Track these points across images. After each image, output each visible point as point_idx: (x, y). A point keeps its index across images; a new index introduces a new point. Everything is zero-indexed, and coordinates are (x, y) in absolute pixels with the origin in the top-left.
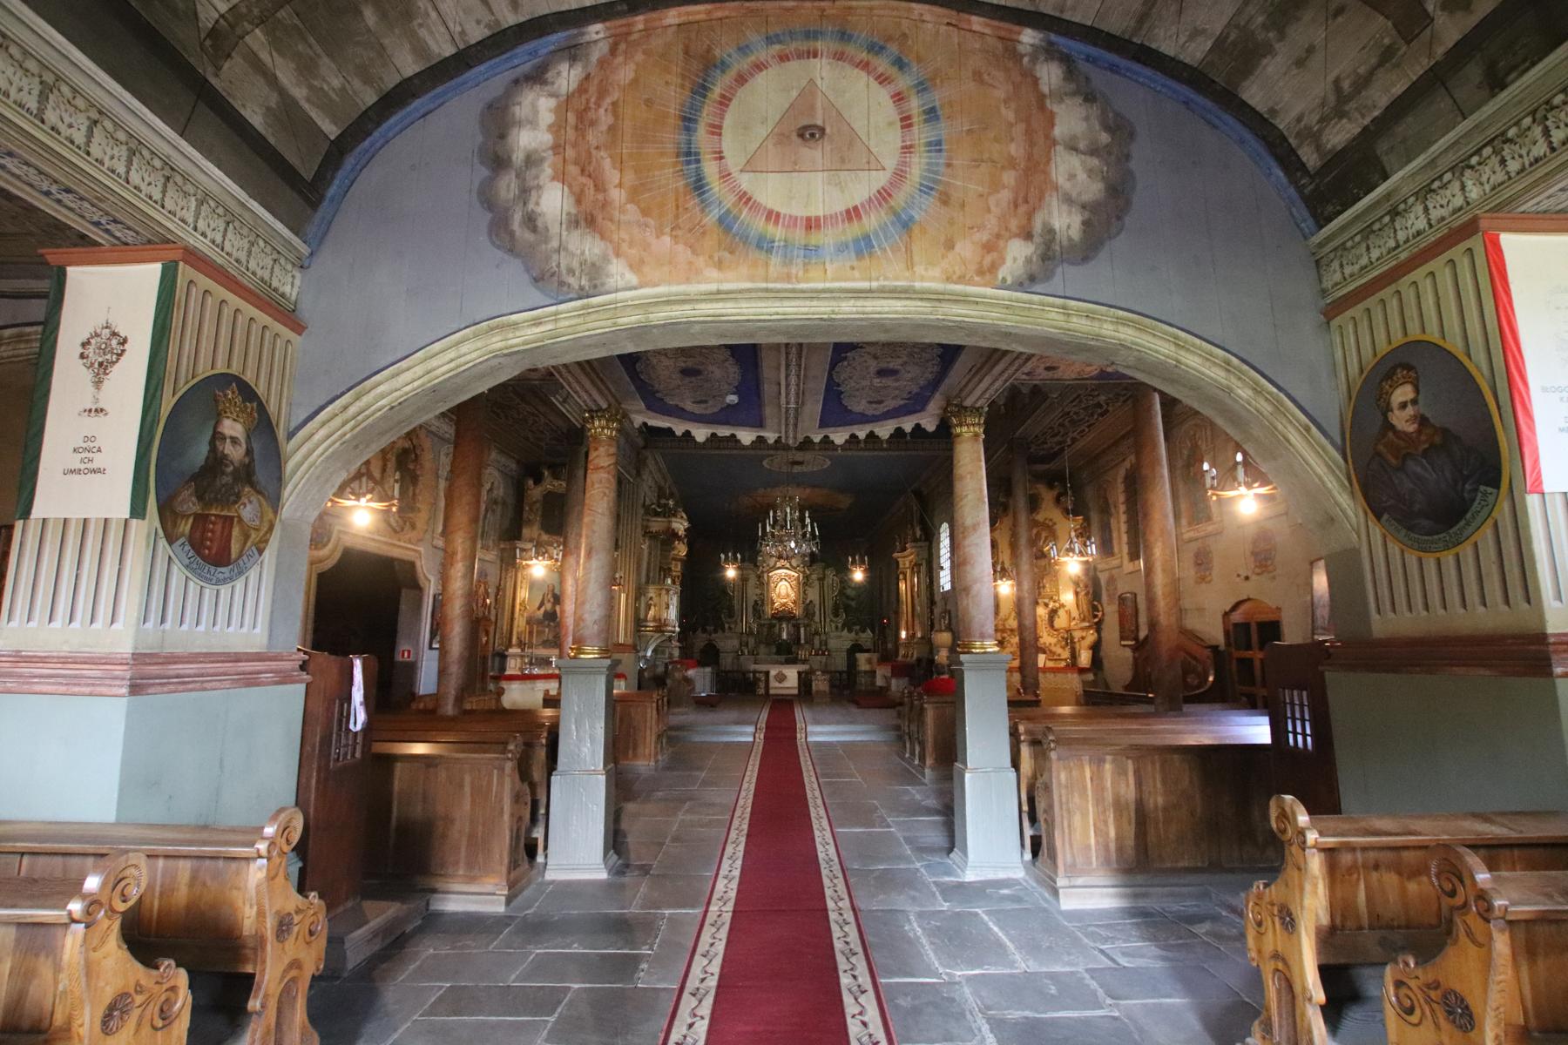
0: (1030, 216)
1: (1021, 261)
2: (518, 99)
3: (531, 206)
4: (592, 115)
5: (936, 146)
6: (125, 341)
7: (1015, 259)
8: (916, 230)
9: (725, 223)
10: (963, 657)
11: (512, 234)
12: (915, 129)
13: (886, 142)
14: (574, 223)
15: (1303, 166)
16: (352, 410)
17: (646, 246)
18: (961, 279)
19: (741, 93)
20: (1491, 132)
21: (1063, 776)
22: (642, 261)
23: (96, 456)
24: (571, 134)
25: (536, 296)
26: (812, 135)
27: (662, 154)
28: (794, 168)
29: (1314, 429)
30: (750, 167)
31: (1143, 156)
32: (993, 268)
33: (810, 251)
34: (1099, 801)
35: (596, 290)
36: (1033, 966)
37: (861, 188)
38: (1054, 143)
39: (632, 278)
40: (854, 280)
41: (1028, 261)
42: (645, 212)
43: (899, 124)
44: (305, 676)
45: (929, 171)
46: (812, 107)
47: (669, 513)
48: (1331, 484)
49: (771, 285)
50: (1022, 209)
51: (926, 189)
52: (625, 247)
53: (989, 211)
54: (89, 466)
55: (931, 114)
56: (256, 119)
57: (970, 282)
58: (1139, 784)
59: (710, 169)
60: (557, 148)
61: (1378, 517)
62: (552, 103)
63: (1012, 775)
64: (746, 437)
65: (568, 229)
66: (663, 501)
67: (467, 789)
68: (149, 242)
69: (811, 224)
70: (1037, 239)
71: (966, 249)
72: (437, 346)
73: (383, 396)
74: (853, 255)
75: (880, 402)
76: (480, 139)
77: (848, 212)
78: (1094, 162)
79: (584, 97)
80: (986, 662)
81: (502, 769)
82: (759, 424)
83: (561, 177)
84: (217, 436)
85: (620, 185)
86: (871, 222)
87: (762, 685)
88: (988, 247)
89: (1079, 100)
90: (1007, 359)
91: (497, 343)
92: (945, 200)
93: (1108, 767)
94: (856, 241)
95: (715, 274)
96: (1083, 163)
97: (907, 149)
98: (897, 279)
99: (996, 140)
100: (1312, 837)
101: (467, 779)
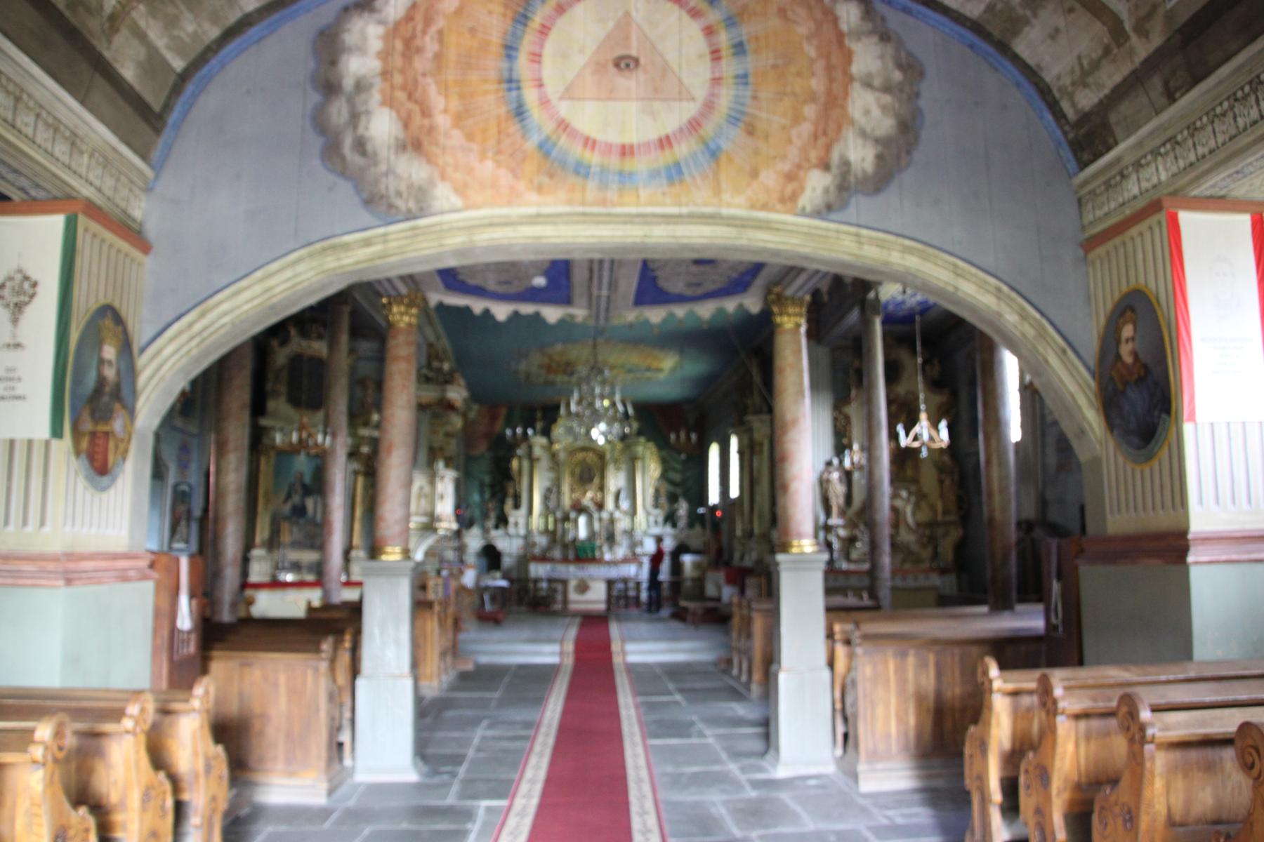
0: (828, 148)
1: (819, 191)
2: (348, 26)
3: (361, 131)
4: (418, 42)
5: (743, 79)
6: (35, 285)
7: (814, 189)
8: (723, 159)
9: (545, 148)
10: (780, 557)
11: (343, 158)
12: (724, 62)
13: (697, 75)
14: (402, 147)
15: (1064, 116)
16: (198, 327)
17: (470, 171)
18: (765, 207)
19: (561, 22)
20: (1169, 133)
21: (868, 670)
22: (466, 185)
23: (18, 385)
24: (398, 61)
25: (365, 217)
26: (628, 66)
27: (486, 81)
28: (611, 95)
29: (1070, 353)
30: (569, 94)
31: (931, 94)
32: (794, 197)
33: (625, 177)
34: (902, 691)
35: (422, 212)
36: (822, 826)
37: (673, 118)
38: (851, 79)
39: (457, 201)
40: (664, 204)
41: (826, 191)
42: (470, 137)
43: (708, 57)
44: (155, 575)
45: (736, 103)
46: (627, 38)
47: (448, 380)
48: (1082, 401)
49: (588, 209)
50: (822, 141)
51: (733, 120)
52: (450, 170)
53: (790, 142)
54: (13, 393)
55: (739, 49)
56: (129, 73)
57: (772, 210)
58: (939, 675)
59: (530, 96)
60: (385, 74)
61: (1112, 432)
62: (380, 30)
63: (826, 674)
64: (552, 314)
65: (397, 153)
66: (435, 364)
67: (283, 690)
68: (55, 198)
69: (626, 151)
70: (835, 170)
71: (770, 178)
72: (274, 267)
73: (225, 314)
74: (664, 181)
75: (699, 285)
76: (312, 64)
77: (660, 140)
78: (887, 99)
79: (410, 25)
80: (803, 560)
81: (316, 670)
82: (567, 301)
83: (389, 102)
84: (101, 361)
85: (445, 111)
86: (682, 150)
87: (559, 597)
88: (790, 177)
89: (875, 39)
90: (803, 277)
91: (330, 262)
92: (751, 131)
93: (911, 660)
94: (668, 168)
95: (533, 197)
96: (878, 100)
97: (716, 81)
98: (705, 205)
99: (799, 74)
100: (997, 684)
101: (282, 679)
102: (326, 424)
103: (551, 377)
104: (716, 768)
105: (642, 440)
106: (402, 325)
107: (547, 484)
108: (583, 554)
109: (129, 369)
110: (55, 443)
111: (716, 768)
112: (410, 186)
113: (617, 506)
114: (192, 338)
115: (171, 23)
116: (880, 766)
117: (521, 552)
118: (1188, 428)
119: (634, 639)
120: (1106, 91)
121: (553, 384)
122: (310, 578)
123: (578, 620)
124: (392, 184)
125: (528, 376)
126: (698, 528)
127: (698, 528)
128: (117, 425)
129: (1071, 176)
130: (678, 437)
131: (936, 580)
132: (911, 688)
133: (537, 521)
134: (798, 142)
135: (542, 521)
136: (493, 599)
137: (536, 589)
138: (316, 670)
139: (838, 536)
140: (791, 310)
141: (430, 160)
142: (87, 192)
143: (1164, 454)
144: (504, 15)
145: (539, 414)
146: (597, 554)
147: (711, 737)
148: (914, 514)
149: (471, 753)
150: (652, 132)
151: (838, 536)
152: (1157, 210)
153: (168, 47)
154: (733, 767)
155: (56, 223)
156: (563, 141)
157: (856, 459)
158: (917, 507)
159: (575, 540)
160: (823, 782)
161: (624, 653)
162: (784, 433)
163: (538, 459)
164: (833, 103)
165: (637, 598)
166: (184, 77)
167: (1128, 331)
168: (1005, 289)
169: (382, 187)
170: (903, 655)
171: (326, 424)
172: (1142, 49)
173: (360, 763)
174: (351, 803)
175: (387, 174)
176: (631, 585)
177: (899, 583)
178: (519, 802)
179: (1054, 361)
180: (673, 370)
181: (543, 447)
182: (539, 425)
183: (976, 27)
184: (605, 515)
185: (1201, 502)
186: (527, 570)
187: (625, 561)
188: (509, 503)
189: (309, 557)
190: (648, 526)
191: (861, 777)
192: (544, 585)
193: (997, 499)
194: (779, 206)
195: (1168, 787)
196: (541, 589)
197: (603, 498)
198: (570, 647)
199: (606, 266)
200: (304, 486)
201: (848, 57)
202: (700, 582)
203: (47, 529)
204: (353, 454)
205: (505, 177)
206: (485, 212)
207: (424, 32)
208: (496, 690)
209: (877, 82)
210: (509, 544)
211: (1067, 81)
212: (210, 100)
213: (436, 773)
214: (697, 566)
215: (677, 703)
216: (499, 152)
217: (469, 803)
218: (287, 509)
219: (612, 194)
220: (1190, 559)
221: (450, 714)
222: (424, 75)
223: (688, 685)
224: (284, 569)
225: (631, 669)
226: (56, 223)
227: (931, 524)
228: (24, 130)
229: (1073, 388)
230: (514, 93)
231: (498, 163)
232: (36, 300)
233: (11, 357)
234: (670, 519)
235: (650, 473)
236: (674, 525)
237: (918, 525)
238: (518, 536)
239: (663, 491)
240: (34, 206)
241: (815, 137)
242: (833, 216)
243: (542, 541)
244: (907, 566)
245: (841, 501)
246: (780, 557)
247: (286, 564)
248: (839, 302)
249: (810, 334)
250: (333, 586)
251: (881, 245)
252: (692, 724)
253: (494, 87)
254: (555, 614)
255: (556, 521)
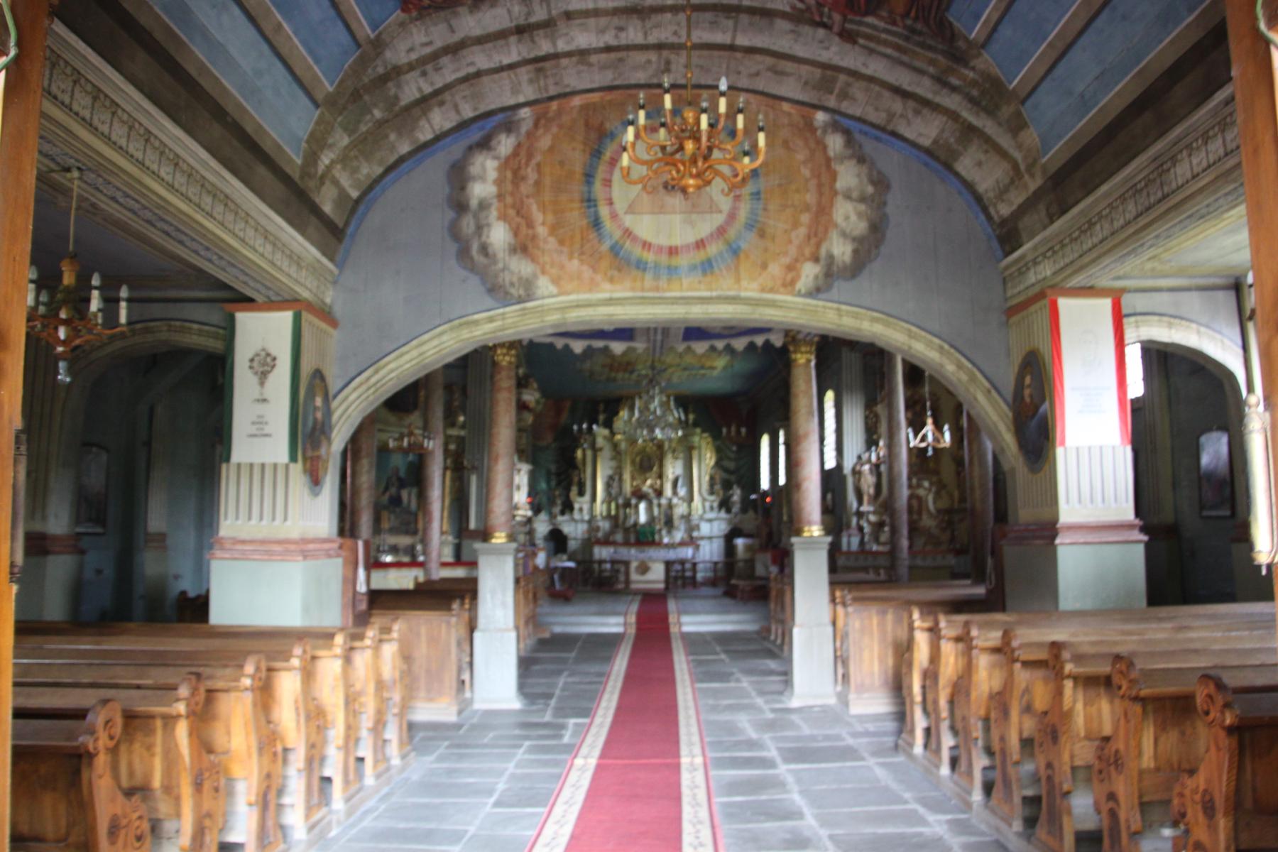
0: (818, 245)
1: (811, 278)
3: (484, 238)
4: (522, 172)
6: (274, 359)
8: (742, 256)
9: (615, 250)
10: (794, 540)
11: (472, 258)
14: (513, 250)
16: (373, 380)
17: (562, 267)
18: (772, 290)
20: (1049, 245)
25: (489, 302)
27: (572, 201)
30: (631, 210)
31: (895, 201)
32: (793, 282)
35: (529, 297)
37: (706, 226)
38: (836, 193)
39: (553, 289)
41: (816, 277)
42: (561, 242)
44: (344, 553)
49: (646, 294)
51: (749, 226)
52: (548, 267)
53: (790, 242)
56: (327, 208)
57: (777, 292)
59: (604, 211)
60: (500, 196)
63: (830, 629)
67: (423, 638)
69: (673, 251)
70: (822, 262)
71: (775, 269)
72: (426, 337)
73: (392, 371)
74: (700, 272)
76: (447, 190)
78: (862, 207)
80: (812, 542)
81: (448, 623)
83: (503, 217)
84: (316, 408)
85: (543, 224)
86: (713, 249)
87: (622, 578)
88: (790, 268)
89: (854, 162)
91: (465, 334)
92: (762, 234)
93: (890, 617)
94: (702, 263)
95: (607, 286)
98: (729, 289)
99: (798, 191)
101: (423, 630)
102: (426, 427)
103: (613, 374)
104: (746, 701)
105: (698, 430)
106: (504, 363)
107: (610, 472)
108: (644, 538)
109: (328, 412)
110: (292, 466)
111: (746, 701)
112: (520, 279)
113: (675, 493)
114: (369, 389)
115: (355, 171)
116: (866, 695)
117: (586, 536)
118: (1060, 451)
119: (687, 612)
120: (1014, 207)
121: (615, 380)
122: (406, 559)
123: (639, 598)
124: (507, 277)
125: (592, 373)
126: (751, 514)
127: (751, 514)
128: (323, 451)
129: (1000, 261)
130: (729, 432)
131: (951, 560)
132: (890, 638)
133: (600, 507)
134: (796, 242)
135: (605, 507)
136: (562, 578)
137: (601, 571)
138: (448, 623)
139: (868, 521)
140: (803, 349)
141: (534, 260)
142: (305, 294)
143: (1047, 467)
144: (584, 151)
145: (602, 407)
146: (657, 537)
147: (745, 683)
148: (935, 502)
149: (558, 692)
150: (690, 237)
151: (868, 521)
152: (1045, 297)
153: (351, 186)
154: (760, 701)
155: (286, 317)
156: (628, 244)
157: (882, 454)
158: (938, 496)
159: (636, 524)
160: (825, 709)
161: (680, 625)
162: (798, 444)
163: (601, 449)
164: (822, 213)
165: (694, 577)
166: (357, 202)
167: (1028, 380)
168: (946, 347)
169: (500, 280)
170: (884, 613)
171: (426, 427)
172: (1033, 184)
173: (477, 696)
174: (475, 720)
175: (503, 270)
176: (688, 566)
177: (919, 562)
178: (598, 720)
179: (981, 397)
180: (725, 368)
181: (605, 437)
182: (601, 417)
183: (928, 151)
184: (664, 501)
185: (1068, 502)
186: (591, 554)
187: (682, 544)
188: (574, 490)
189: (404, 541)
190: (704, 512)
191: (851, 703)
192: (608, 566)
193: (978, 493)
194: (782, 290)
195: (990, 676)
196: (606, 570)
197: (662, 485)
198: (632, 619)
199: (659, 332)
200: (400, 479)
201: (834, 176)
202: (750, 563)
203: (289, 523)
204: (446, 452)
205: (587, 272)
206: (573, 297)
207: (527, 165)
208: (571, 651)
209: (855, 195)
210: (574, 529)
211: (991, 195)
212: (375, 218)
213: (533, 703)
214: (748, 548)
215: (722, 661)
216: (582, 253)
217: (561, 721)
218: (385, 499)
219: (663, 283)
220: (1058, 541)
221: (536, 667)
222: (528, 197)
223: (732, 648)
224: (384, 552)
225: (686, 637)
226: (286, 317)
227: (949, 511)
228: (60, 96)
229: (995, 418)
230: (592, 210)
231: (582, 261)
232: (276, 371)
233: (260, 409)
234: (725, 504)
235: (705, 463)
236: (728, 511)
237: (939, 511)
238: (582, 521)
239: (718, 478)
240: (273, 305)
241: (809, 237)
242: (821, 296)
243: (605, 525)
244: (929, 548)
245: (872, 491)
246: (794, 540)
247: (386, 548)
248: (831, 350)
249: (818, 366)
250: (433, 565)
251: (856, 316)
252: (732, 674)
253: (577, 205)
254: (617, 593)
255: (617, 507)
